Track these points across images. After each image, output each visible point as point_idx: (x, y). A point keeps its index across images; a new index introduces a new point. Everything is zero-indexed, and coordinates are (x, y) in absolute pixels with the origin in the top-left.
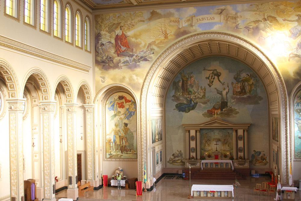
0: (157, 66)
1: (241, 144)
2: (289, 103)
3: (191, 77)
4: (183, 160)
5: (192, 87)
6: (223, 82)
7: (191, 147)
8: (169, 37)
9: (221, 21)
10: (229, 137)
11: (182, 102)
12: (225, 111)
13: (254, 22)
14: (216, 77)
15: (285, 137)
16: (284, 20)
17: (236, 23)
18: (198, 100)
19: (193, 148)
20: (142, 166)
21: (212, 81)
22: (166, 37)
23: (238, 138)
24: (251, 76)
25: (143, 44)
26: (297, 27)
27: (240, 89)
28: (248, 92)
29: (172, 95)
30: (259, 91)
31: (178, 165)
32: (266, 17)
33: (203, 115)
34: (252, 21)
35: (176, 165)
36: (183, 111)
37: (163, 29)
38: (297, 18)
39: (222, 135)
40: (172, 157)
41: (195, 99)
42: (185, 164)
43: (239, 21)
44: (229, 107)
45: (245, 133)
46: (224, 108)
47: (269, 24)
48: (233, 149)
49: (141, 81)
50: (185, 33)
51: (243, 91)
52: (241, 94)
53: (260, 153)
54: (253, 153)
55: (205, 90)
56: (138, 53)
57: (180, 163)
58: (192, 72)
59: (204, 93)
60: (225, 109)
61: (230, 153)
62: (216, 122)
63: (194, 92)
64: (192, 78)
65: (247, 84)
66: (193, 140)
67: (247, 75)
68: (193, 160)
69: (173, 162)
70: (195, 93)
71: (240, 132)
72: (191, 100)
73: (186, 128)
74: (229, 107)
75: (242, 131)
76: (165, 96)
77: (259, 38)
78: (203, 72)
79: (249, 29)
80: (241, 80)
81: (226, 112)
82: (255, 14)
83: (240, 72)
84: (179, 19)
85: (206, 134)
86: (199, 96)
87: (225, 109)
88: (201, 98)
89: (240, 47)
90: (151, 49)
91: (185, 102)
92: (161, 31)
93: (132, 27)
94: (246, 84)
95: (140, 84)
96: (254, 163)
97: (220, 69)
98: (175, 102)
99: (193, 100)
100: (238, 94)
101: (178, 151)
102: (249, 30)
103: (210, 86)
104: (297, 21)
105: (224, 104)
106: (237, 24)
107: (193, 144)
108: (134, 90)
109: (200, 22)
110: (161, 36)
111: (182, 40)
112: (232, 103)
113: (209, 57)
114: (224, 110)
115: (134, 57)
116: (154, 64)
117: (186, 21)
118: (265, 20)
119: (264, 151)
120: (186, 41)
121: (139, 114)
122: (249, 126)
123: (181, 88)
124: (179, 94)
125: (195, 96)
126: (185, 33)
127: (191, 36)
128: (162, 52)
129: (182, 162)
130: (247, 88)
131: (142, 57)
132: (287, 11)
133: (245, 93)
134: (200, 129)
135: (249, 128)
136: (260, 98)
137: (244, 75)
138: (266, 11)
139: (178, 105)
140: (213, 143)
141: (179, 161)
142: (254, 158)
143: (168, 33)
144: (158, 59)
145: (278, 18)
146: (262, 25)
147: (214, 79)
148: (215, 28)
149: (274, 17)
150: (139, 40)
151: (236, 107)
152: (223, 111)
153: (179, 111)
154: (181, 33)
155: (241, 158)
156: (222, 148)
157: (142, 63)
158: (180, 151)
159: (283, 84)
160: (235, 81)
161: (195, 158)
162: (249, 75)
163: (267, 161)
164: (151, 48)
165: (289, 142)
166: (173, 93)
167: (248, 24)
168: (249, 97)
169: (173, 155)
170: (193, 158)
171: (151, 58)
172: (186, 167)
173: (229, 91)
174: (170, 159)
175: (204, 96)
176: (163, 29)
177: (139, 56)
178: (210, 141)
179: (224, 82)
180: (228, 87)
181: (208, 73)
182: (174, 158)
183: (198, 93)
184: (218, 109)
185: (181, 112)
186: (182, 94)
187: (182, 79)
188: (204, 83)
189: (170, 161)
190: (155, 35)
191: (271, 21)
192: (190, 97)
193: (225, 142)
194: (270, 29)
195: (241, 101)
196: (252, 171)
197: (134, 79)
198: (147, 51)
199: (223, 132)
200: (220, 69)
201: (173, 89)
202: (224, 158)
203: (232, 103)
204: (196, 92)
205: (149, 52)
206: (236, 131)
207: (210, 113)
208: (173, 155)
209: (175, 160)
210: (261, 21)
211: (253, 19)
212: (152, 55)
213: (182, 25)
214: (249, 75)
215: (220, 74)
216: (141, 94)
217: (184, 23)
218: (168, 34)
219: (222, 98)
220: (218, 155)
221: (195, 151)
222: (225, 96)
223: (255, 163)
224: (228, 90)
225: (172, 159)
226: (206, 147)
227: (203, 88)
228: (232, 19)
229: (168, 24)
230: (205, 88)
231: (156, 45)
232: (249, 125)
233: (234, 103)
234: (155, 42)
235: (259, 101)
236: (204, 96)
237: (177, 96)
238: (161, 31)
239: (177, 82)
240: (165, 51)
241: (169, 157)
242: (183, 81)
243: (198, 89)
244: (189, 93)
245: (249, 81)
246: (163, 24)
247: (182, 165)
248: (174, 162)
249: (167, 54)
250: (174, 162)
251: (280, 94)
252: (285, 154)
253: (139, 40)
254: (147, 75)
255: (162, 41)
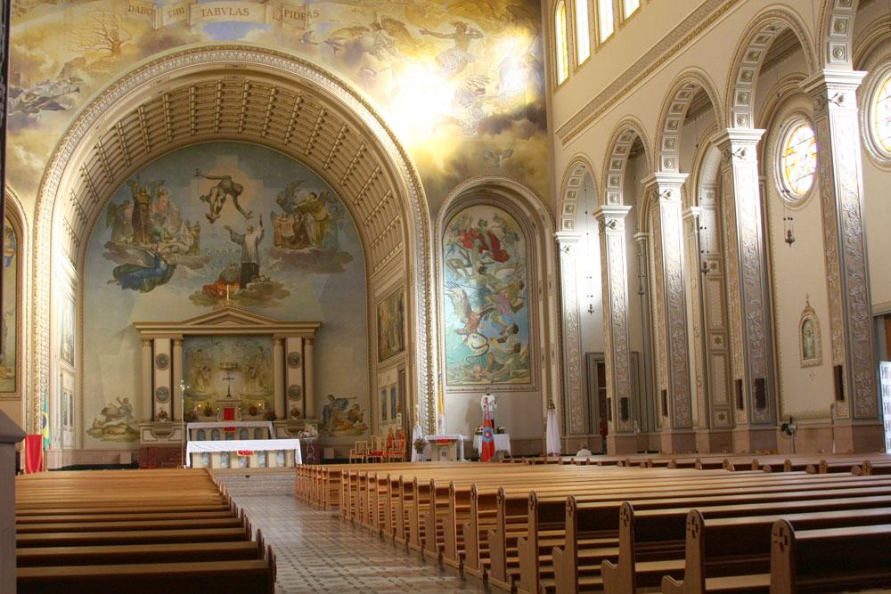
0: (88, 125)
1: (295, 376)
2: (434, 236)
3: (160, 195)
4: (133, 427)
5: (162, 221)
6: (247, 211)
7: (158, 385)
8: (126, 51)
9: (265, 19)
10: (263, 358)
11: (132, 263)
12: (251, 289)
13: (349, 29)
14: (229, 197)
15: (424, 322)
16: (423, 33)
17: (304, 29)
18: (177, 258)
19: (163, 389)
20: (35, 404)
21: (218, 207)
22: (115, 49)
23: (289, 361)
24: (323, 199)
25: (49, 63)
26: (454, 52)
27: (292, 230)
28: (315, 238)
29: (104, 242)
30: (342, 237)
31: (118, 441)
32: (379, 21)
33: (191, 298)
34: (345, 27)
35: (113, 440)
36: (135, 288)
37: (109, 27)
38: (453, 30)
39: (242, 355)
40: (102, 418)
41: (169, 254)
42: (139, 438)
43: (313, 25)
44: (263, 279)
45: (308, 348)
46: (249, 281)
47: (386, 39)
48: (272, 393)
49: (39, 164)
50: (168, 42)
51: (301, 237)
52: (297, 245)
53: (346, 402)
54: (328, 402)
55: (198, 231)
56: (33, 86)
57: (124, 433)
58: (163, 182)
59: (196, 238)
60: (253, 284)
61: (267, 404)
62: (228, 315)
63: (166, 236)
64: (164, 198)
65: (312, 218)
66: (162, 366)
67: (312, 196)
68: (163, 421)
69: (104, 433)
70: (171, 239)
71: (294, 345)
72: (158, 258)
73: (142, 332)
74: (263, 279)
75: (299, 340)
76: (83, 242)
77: (362, 69)
78: (194, 182)
79: (338, 47)
80: (296, 207)
81: (254, 291)
82: (353, 11)
83: (294, 187)
84: (155, 4)
85: (199, 351)
86: (181, 246)
87: (253, 284)
88: (187, 253)
89: (310, 89)
90: (70, 79)
91: (141, 262)
92: (101, 31)
93: (20, 16)
94: (310, 217)
95: (34, 172)
96: (330, 431)
97: (240, 177)
98: (111, 261)
99: (164, 256)
100: (288, 244)
101: (118, 399)
102: (335, 49)
103: (212, 221)
104: (454, 36)
105: (249, 271)
106: (307, 31)
107: (163, 378)
108: (16, 189)
109: (211, 17)
110: (103, 46)
111: (160, 61)
112: (269, 269)
113: (211, 143)
114: (248, 285)
115: (22, 97)
116: (79, 119)
117: (172, 14)
118: (377, 27)
119: (355, 398)
120: (171, 64)
121: (30, 255)
122: (316, 329)
123: (130, 223)
124: (123, 238)
125: (170, 247)
126: (168, 42)
127: (186, 53)
128: (101, 90)
129: (129, 430)
130: (312, 231)
131: (43, 99)
132: (430, 11)
133: (306, 242)
134: (184, 335)
135: (316, 335)
136: (347, 257)
137: (303, 196)
138: (382, 7)
139: (121, 271)
140: (218, 376)
141: (122, 430)
142: (330, 416)
143: (121, 39)
144: (91, 105)
145: (409, 27)
146: (369, 39)
147: (223, 201)
148: (250, 38)
149: (398, 22)
150: (37, 52)
151: (282, 279)
152: (245, 288)
153: (123, 288)
154: (157, 43)
155: (296, 413)
156: (245, 390)
157: (44, 116)
158: (126, 400)
159: (418, 189)
160: (279, 210)
161: (168, 416)
162: (318, 195)
163: (364, 425)
164: (72, 76)
165: (433, 334)
166: (106, 235)
167: (334, 33)
168: (317, 254)
169: (104, 411)
170: (163, 415)
171: (70, 102)
172: (142, 442)
173: (262, 236)
174: (94, 423)
175: (195, 246)
176: (109, 27)
177: (36, 95)
178: (209, 370)
179: (251, 212)
180: (261, 223)
181: (206, 186)
182: (108, 420)
183: (179, 240)
184: (232, 284)
185: (131, 290)
186: (131, 239)
187: (134, 198)
188: (196, 211)
189: (95, 428)
190: (84, 43)
191: (393, 31)
192: (154, 248)
193: (252, 373)
194: (390, 52)
195: (292, 262)
196: (325, 449)
197: (18, 156)
198: (59, 84)
199: (246, 345)
200: (240, 177)
201: (108, 226)
202: (249, 417)
203: (271, 268)
204: (173, 236)
205: (66, 85)
206: (283, 342)
207: (212, 294)
208: (104, 411)
209: (108, 427)
210: (368, 30)
211: (347, 23)
212: (74, 96)
213: (162, 23)
214: (318, 195)
215: (239, 190)
216: (38, 200)
217: (165, 17)
218: (121, 43)
219: (245, 254)
220: (233, 409)
221: (170, 397)
222: (253, 249)
223: (332, 431)
224: (260, 233)
225: (100, 423)
226: (199, 389)
227: (192, 225)
228: (295, 18)
229: (124, 16)
230: (198, 226)
231: (85, 69)
232: (318, 325)
233: (278, 269)
234: (83, 60)
235: (343, 265)
236: (195, 246)
237: (117, 244)
238: (101, 31)
239: (119, 204)
240: (112, 87)
241: (93, 416)
242: (137, 204)
243: (179, 228)
244: (154, 237)
245: (316, 212)
246: (110, 13)
247: (128, 440)
248: (106, 431)
249: (116, 94)
250: (109, 433)
251: (412, 211)
252: (426, 365)
253: (37, 52)
254: (58, 149)
255: (104, 59)
